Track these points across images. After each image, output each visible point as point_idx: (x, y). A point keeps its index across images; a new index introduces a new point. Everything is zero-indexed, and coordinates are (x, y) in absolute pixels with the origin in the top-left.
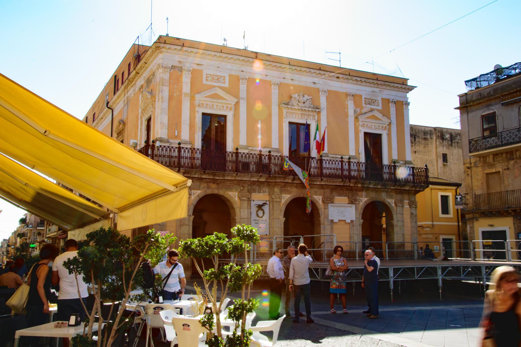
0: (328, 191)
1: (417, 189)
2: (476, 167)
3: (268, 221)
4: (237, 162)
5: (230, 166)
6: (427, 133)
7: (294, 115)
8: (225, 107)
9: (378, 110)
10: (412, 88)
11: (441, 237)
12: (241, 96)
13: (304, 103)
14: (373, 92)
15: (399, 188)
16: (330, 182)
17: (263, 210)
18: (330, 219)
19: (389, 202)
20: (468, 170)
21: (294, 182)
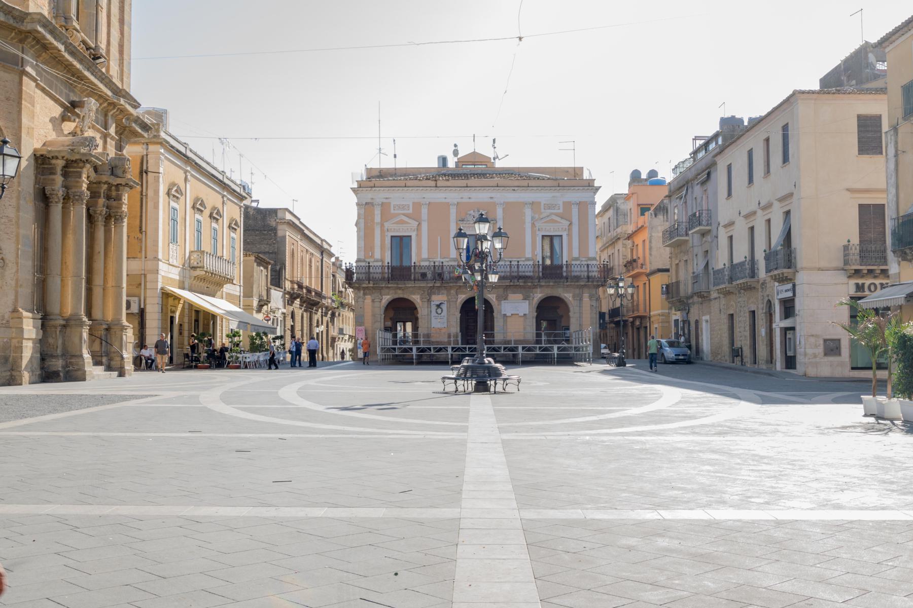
0: (501, 290)
4: (434, 273)
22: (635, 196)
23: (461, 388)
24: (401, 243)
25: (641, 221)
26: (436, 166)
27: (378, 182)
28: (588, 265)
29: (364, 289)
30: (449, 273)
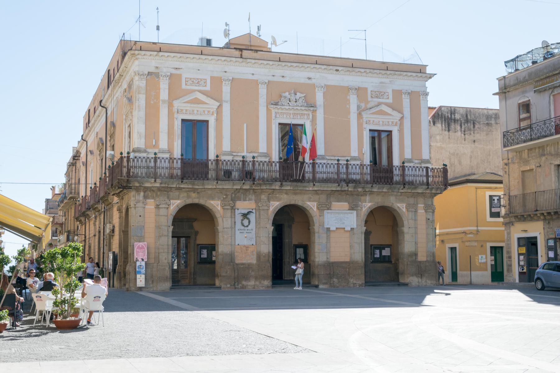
0: (323, 197)
1: (434, 191)
2: (513, 163)
3: (254, 230)
5: (212, 174)
6: (491, 117)
7: (285, 116)
8: (206, 112)
9: (386, 104)
10: (431, 76)
11: (489, 245)
12: (223, 99)
13: (296, 102)
14: (381, 83)
15: (410, 191)
17: (248, 219)
18: (325, 227)
19: (398, 207)
20: (505, 166)
21: (283, 188)
24: (195, 131)
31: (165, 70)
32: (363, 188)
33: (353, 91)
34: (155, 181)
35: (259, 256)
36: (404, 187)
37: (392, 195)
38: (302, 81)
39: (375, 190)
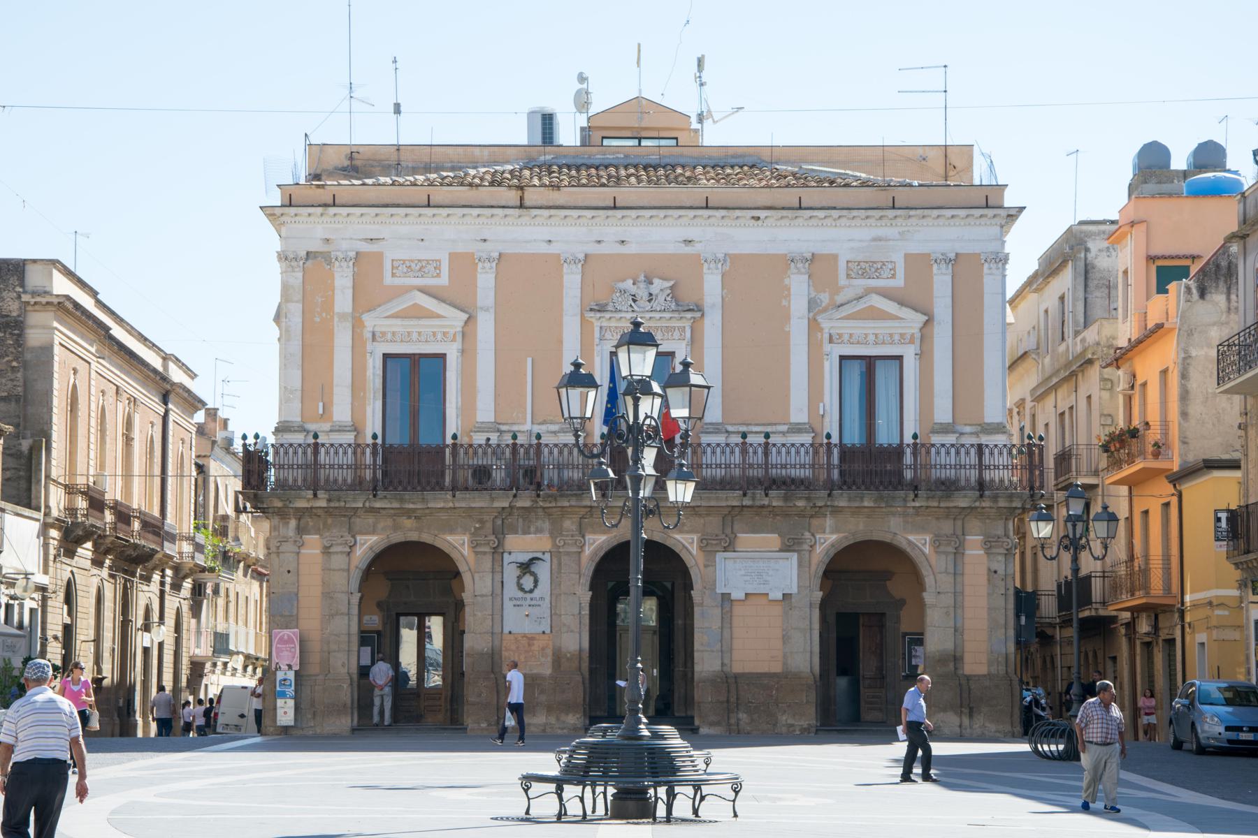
4: (512, 466)
8: (439, 337)
12: (479, 304)
13: (650, 301)
15: (936, 504)
16: (709, 499)
17: (534, 574)
18: (718, 591)
19: (910, 542)
22: (1140, 231)
23: (574, 808)
24: (415, 378)
25: (1163, 307)
26: (523, 140)
27: (347, 187)
28: (980, 449)
29: (301, 513)
30: (560, 467)
31: (345, 245)
32: (808, 499)
33: (800, 265)
34: (315, 495)
35: (558, 658)
36: (916, 496)
37: (893, 514)
38: (671, 249)
39: (842, 503)
